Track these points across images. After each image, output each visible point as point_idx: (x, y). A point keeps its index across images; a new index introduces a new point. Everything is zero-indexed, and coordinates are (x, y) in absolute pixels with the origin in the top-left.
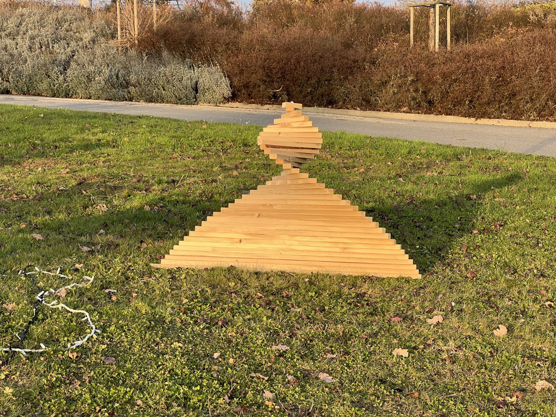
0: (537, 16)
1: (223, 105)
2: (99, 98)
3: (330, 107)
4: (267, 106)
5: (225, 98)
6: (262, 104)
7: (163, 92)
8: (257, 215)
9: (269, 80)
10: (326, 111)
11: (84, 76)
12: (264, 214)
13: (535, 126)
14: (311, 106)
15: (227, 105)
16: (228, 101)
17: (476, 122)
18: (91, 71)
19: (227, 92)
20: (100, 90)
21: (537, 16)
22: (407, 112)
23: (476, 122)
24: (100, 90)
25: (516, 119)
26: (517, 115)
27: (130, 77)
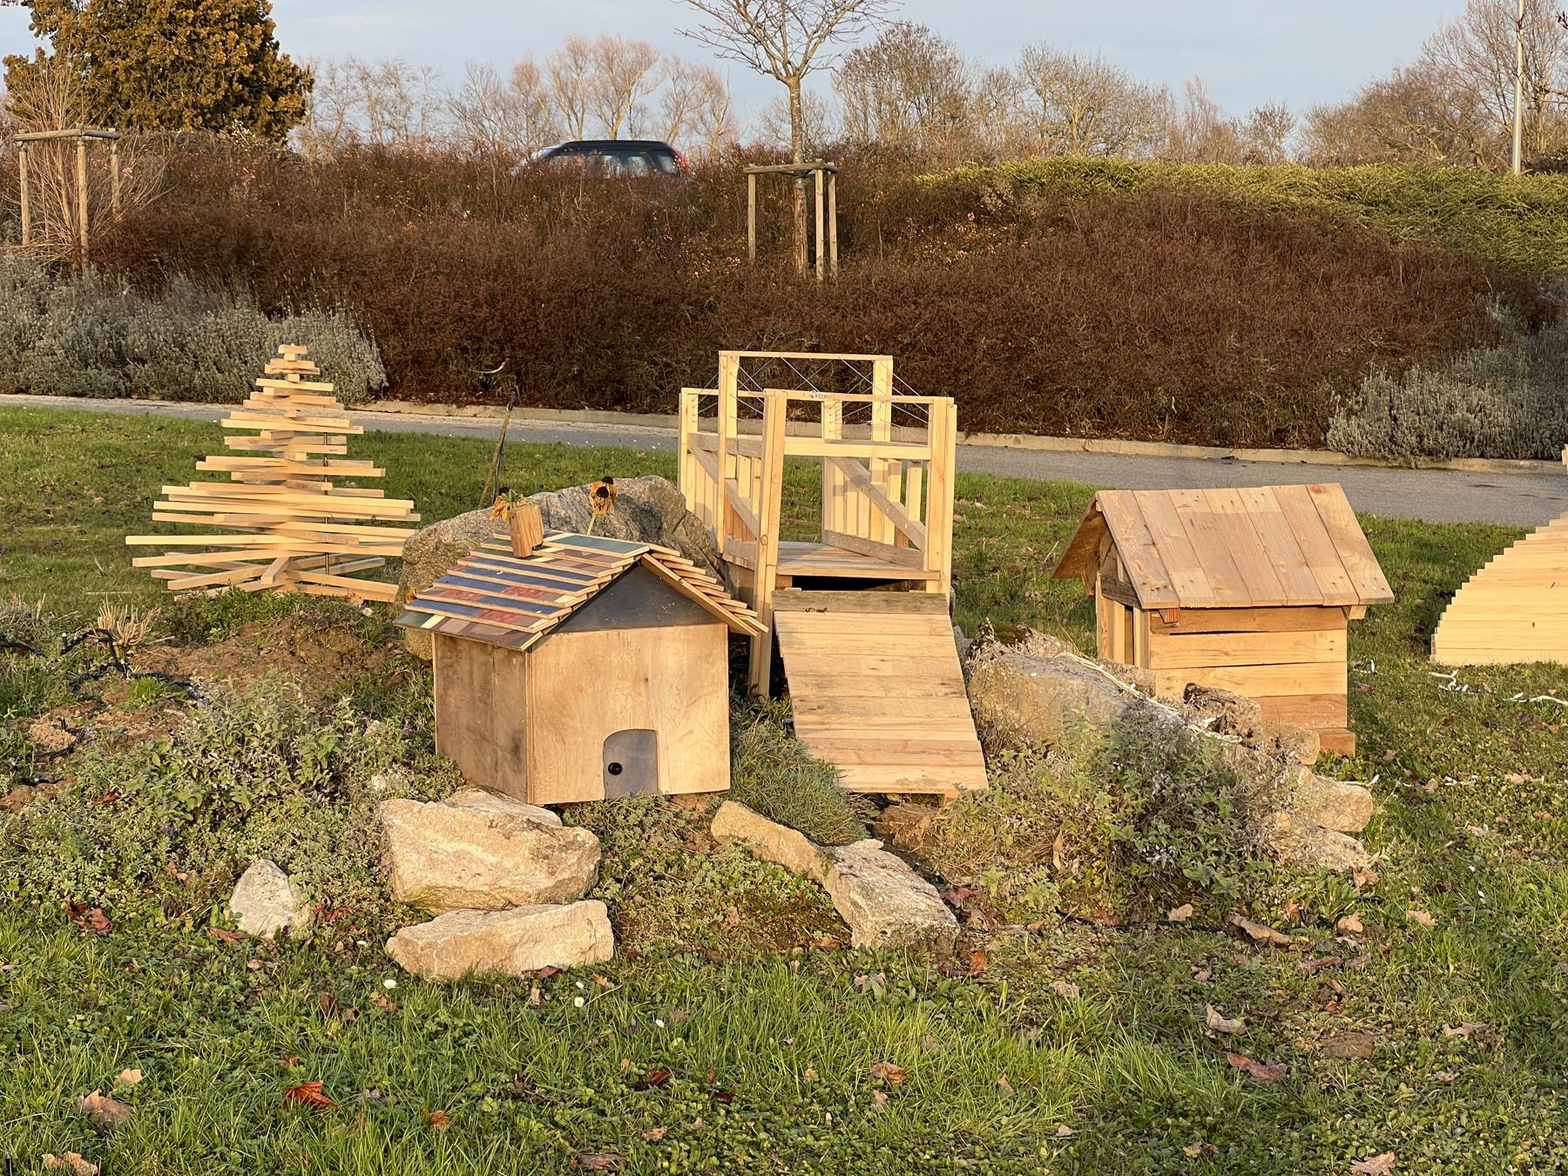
0: (1000, 196)
1: (362, 407)
2: (50, 390)
3: (619, 408)
4: (471, 409)
5: (370, 389)
6: (461, 404)
7: (219, 376)
8: (1550, 584)
9: (472, 348)
10: (615, 420)
11: (9, 335)
12: (1562, 582)
13: (1097, 449)
14: (575, 408)
15: (373, 407)
16: (377, 398)
17: (967, 442)
18: (24, 325)
19: (377, 374)
20: (52, 371)
21: (1000, 196)
22: (805, 420)
23: (967, 442)
24: (52, 371)
25: (1051, 435)
26: (1055, 428)
27: (1329, 435)
